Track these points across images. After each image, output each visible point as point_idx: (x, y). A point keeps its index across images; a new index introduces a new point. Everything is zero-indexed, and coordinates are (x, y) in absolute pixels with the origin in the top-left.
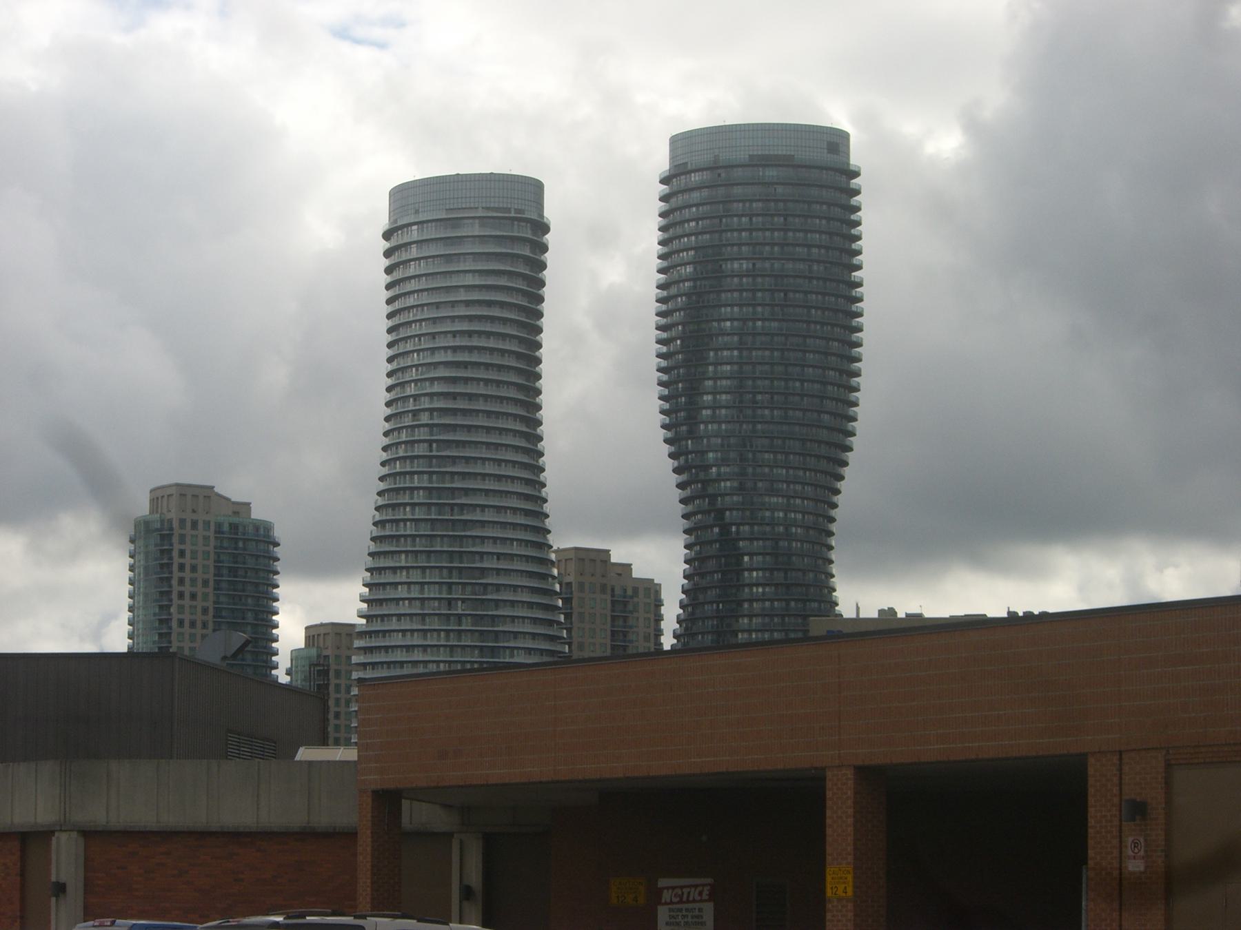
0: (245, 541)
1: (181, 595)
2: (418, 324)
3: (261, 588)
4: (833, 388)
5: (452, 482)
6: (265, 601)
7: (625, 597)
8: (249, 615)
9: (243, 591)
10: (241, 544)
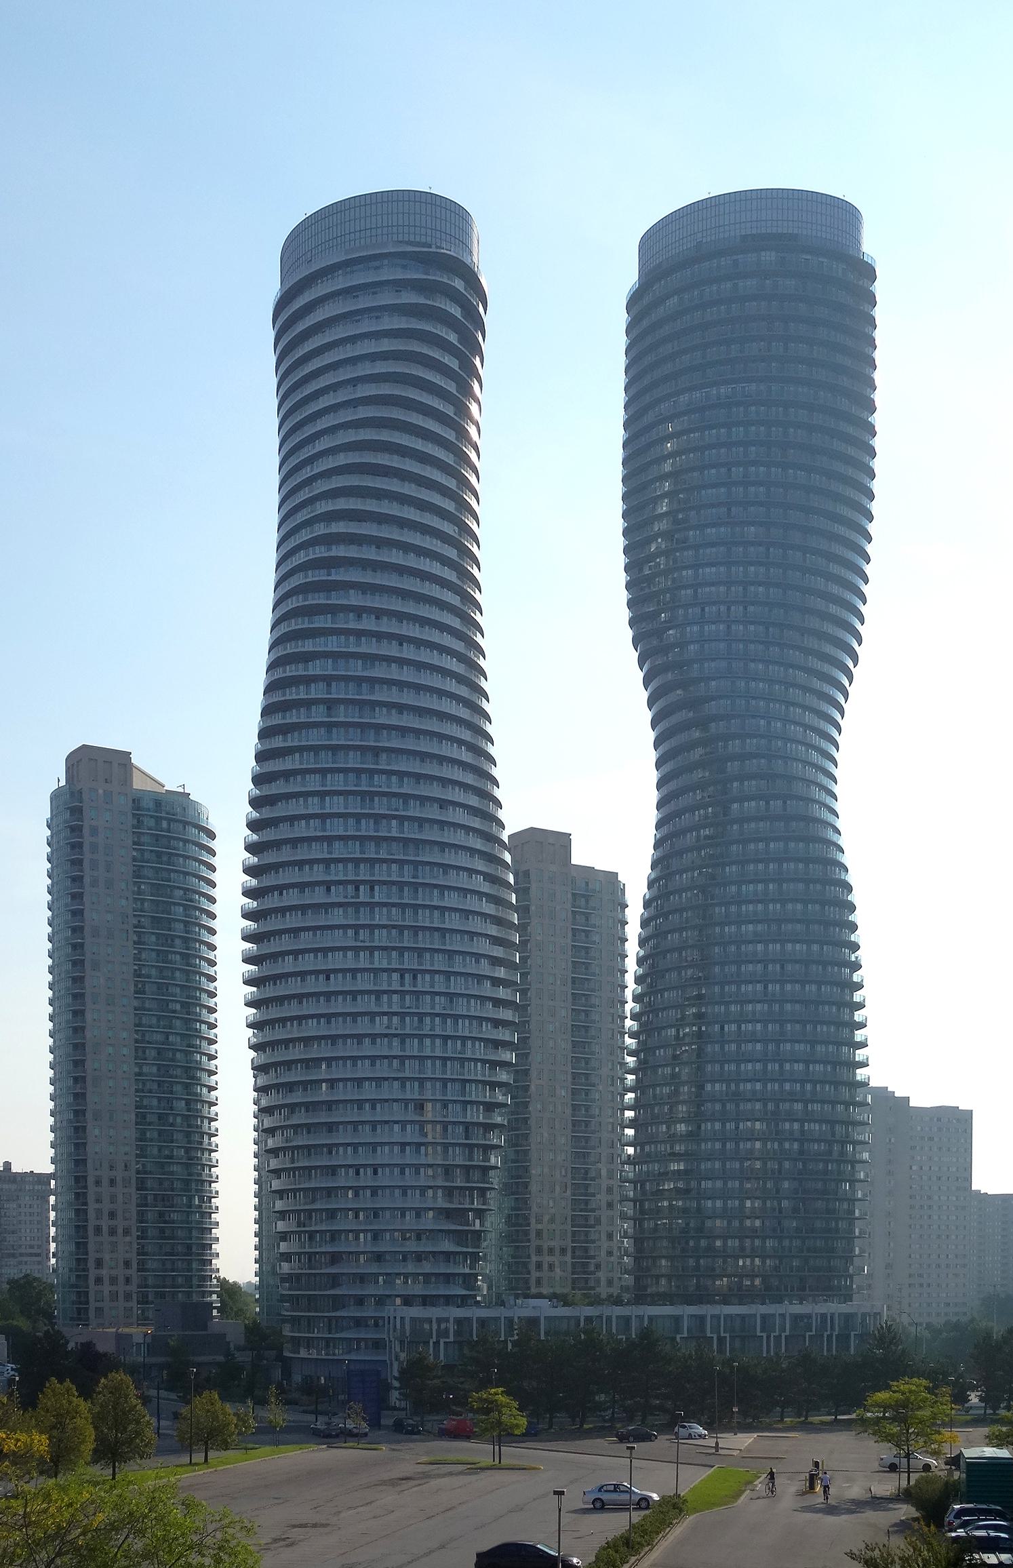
0: (169, 821)
1: (98, 1230)
2: (315, 1020)
3: (193, 1154)
4: (650, 1146)
5: (389, 764)
6: (198, 1008)
7: (587, 890)
8: (179, 1120)
9: (173, 1060)
10: (165, 824)
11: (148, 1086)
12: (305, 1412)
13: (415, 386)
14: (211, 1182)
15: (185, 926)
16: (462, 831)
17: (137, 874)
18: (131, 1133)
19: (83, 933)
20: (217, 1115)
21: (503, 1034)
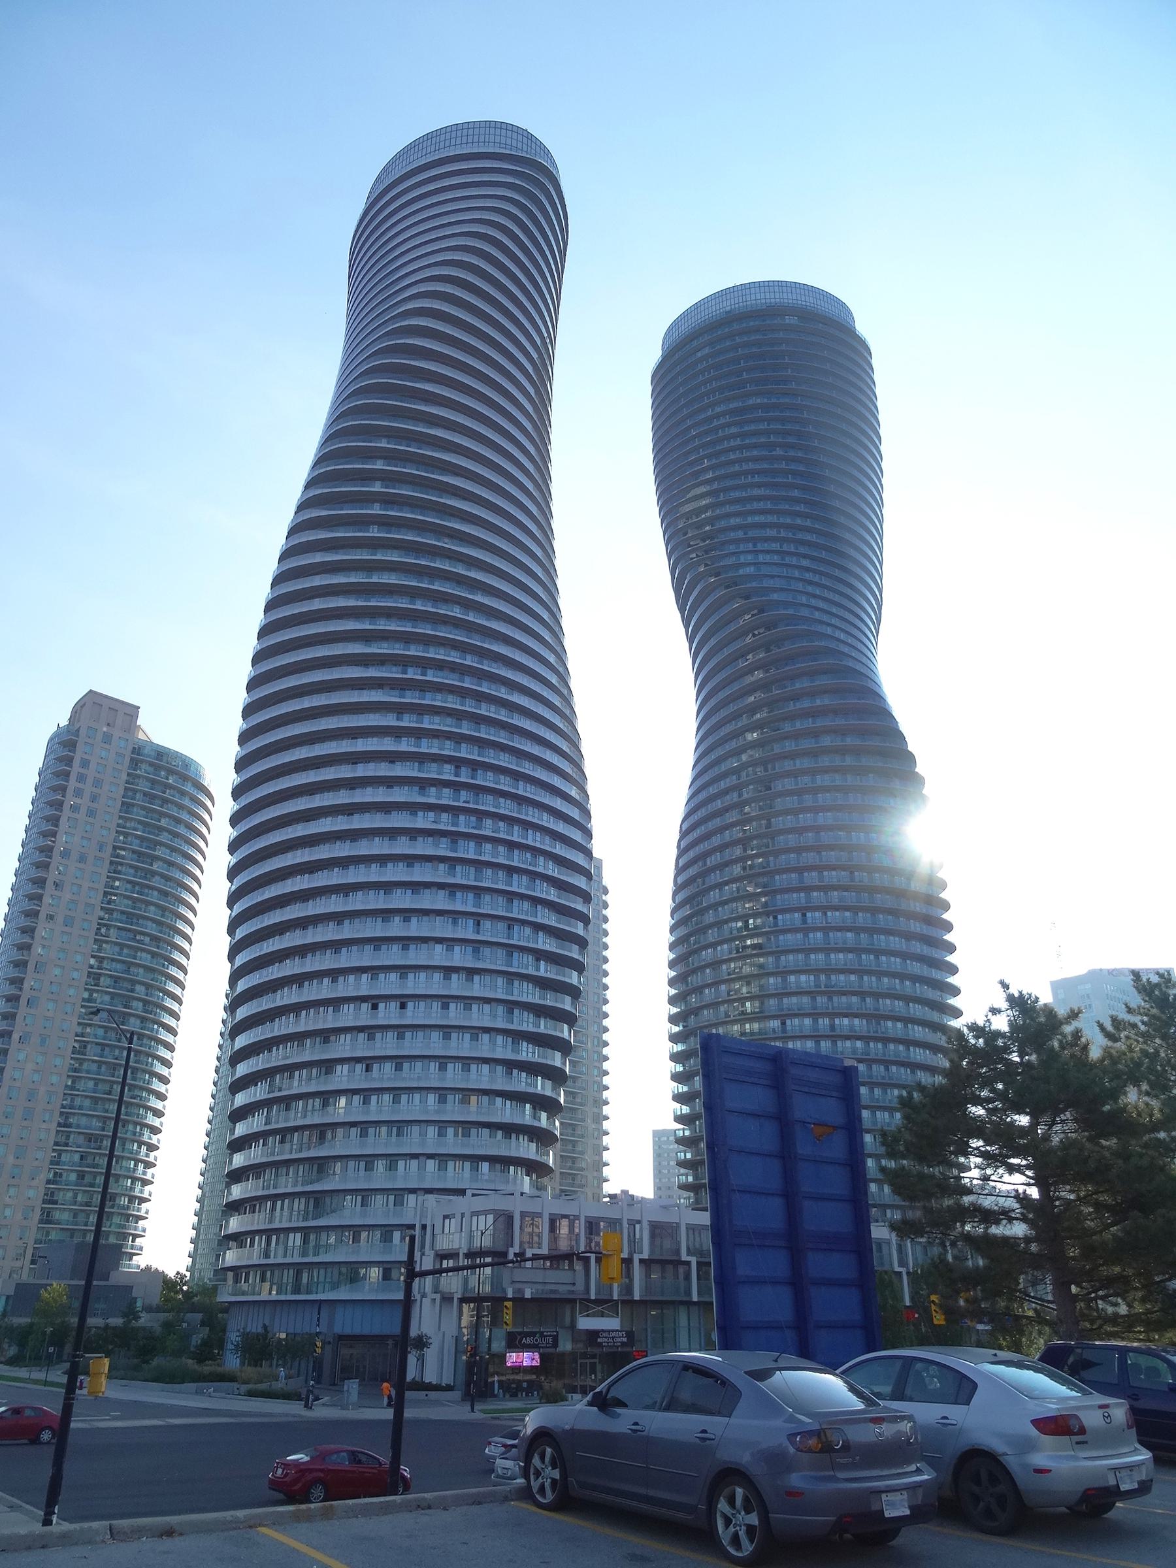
11: (78, 1101)
12: (251, 1394)
13: (451, 537)
14: (135, 1236)
15: (144, 1005)
16: (526, 1137)
17: (126, 806)
18: (63, 1062)
19: (6, 1056)
20: (144, 1231)
21: (545, 943)
